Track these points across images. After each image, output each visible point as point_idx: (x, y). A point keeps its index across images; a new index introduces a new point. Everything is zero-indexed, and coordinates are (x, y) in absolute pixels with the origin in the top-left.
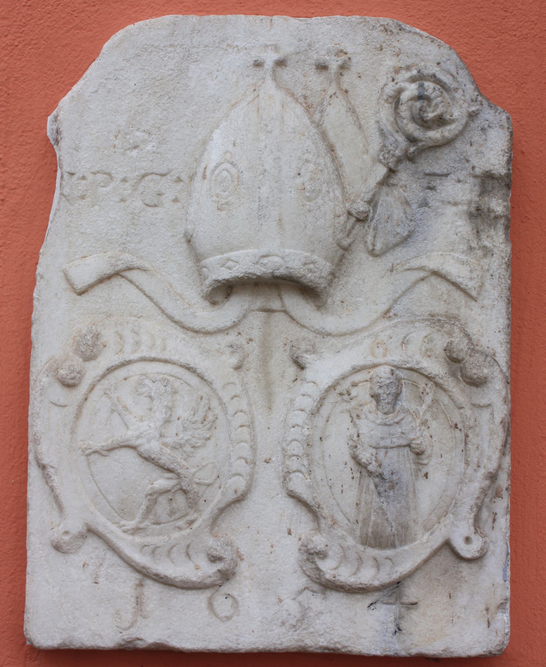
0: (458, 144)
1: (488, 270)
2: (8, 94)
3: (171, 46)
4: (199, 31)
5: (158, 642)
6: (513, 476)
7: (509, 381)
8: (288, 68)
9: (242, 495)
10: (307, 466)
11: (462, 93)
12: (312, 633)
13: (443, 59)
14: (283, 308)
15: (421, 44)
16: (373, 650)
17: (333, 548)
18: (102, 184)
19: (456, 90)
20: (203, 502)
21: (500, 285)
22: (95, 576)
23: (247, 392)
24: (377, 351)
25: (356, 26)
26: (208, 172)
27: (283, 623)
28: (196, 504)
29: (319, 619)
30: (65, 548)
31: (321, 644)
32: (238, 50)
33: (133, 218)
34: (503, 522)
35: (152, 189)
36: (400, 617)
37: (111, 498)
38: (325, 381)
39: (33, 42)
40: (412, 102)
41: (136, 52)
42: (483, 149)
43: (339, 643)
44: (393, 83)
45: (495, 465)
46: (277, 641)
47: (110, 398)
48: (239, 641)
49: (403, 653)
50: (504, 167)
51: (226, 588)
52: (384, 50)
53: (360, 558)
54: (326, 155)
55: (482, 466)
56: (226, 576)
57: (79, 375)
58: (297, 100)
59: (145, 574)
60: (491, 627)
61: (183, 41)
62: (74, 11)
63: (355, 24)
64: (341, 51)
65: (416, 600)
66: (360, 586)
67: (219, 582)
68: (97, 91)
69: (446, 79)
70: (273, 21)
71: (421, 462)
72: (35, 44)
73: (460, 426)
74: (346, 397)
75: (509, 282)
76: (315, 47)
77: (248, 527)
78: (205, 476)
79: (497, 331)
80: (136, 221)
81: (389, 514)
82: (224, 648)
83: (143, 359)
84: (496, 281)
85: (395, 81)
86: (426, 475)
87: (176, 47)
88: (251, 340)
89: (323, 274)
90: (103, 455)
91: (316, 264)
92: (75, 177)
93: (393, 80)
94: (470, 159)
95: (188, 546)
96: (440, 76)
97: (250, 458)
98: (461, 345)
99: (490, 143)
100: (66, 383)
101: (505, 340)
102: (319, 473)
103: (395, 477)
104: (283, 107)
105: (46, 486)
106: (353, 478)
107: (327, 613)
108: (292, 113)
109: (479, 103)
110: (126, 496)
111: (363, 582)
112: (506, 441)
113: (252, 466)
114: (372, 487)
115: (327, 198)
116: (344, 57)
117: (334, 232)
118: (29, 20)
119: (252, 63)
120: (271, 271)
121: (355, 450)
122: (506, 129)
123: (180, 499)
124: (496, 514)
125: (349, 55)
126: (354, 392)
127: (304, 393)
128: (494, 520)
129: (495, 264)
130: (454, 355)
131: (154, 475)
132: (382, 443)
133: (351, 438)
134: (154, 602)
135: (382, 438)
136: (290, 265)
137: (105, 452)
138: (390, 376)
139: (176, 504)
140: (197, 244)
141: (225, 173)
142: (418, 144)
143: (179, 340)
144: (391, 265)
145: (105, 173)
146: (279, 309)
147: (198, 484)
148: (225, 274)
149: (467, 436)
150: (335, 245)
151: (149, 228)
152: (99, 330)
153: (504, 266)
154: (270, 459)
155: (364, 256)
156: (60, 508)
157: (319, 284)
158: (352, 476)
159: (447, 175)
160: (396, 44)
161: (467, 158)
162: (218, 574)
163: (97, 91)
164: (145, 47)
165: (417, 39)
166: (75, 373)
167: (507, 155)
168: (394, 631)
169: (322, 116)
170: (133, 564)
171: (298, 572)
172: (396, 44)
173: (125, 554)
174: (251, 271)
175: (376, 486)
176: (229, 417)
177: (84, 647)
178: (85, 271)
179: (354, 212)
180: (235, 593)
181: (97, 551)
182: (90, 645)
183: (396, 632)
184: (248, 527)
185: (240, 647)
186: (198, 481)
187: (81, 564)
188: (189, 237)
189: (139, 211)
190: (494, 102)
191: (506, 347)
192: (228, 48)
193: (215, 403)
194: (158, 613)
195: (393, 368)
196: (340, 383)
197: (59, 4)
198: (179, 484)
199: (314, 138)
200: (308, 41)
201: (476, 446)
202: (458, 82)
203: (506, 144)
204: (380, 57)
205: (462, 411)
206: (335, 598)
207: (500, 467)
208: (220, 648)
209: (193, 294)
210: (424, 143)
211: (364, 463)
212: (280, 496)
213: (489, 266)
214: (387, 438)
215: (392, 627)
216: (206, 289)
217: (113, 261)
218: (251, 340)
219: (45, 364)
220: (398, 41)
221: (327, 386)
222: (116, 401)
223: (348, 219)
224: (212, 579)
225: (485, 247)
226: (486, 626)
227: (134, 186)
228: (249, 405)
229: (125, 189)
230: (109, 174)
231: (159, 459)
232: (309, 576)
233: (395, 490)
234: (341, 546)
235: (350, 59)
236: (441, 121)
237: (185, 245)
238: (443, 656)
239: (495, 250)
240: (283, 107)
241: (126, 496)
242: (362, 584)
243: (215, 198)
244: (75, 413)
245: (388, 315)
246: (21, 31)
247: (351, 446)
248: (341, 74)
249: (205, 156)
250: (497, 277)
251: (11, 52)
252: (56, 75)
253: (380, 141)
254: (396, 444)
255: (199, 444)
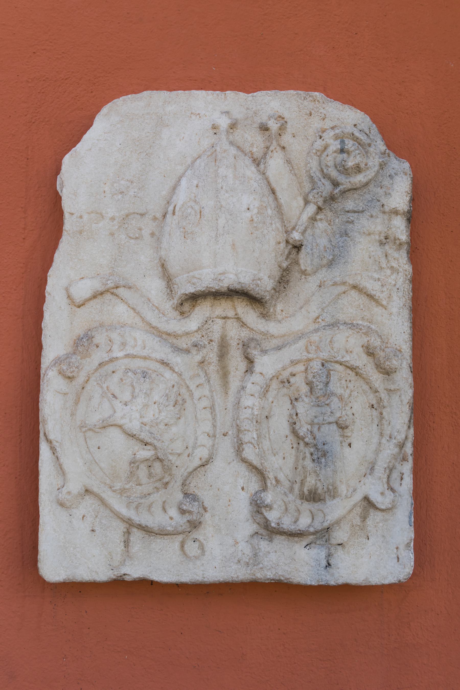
0: (371, 187)
1: (395, 285)
2: (28, 159)
3: (148, 114)
4: (169, 102)
5: (142, 576)
6: (416, 445)
7: (412, 370)
8: (238, 130)
9: (206, 461)
10: (256, 439)
11: (374, 148)
12: (261, 568)
13: (359, 122)
14: (236, 316)
15: (342, 111)
16: (309, 581)
17: (277, 503)
18: (95, 222)
19: (370, 145)
20: (176, 468)
21: (404, 297)
22: (92, 525)
23: (209, 381)
24: (310, 348)
25: (291, 97)
26: (177, 209)
27: (239, 561)
28: (170, 469)
29: (267, 557)
30: (68, 504)
31: (269, 577)
32: (200, 117)
33: (119, 247)
34: (408, 481)
35: (134, 225)
36: (329, 555)
37: (102, 465)
38: (270, 371)
39: (46, 120)
40: (336, 154)
41: (121, 119)
42: (390, 191)
43: (283, 576)
44: (321, 140)
45: (403, 436)
46: (234, 575)
47: (101, 387)
48: (205, 576)
49: (332, 583)
50: (407, 205)
51: (195, 535)
52: (313, 116)
53: (299, 510)
54: (269, 195)
55: (393, 437)
56: (195, 525)
57: (77, 370)
58: (246, 155)
59: (130, 525)
60: (400, 562)
61: (157, 110)
62: (76, 96)
63: (290, 96)
64: (280, 117)
65: (342, 542)
66: (299, 532)
67: (189, 530)
68: (90, 149)
69: (363, 137)
70: (227, 95)
71: (345, 434)
72: (47, 121)
73: (375, 406)
74: (287, 384)
75: (411, 294)
76: (259, 114)
77: (211, 486)
78: (178, 446)
79: (402, 332)
80: (122, 250)
81: (321, 476)
82: (193, 581)
83: (127, 356)
84: (401, 294)
85: (322, 139)
86: (350, 445)
87: (152, 115)
88: (211, 341)
89: (268, 289)
90: (95, 432)
91: (262, 281)
92: (74, 216)
93: (321, 137)
94: (380, 199)
95: (164, 502)
96: (357, 134)
97: (211, 433)
98: (376, 342)
99: (396, 186)
100: (67, 376)
101: (408, 339)
102: (266, 444)
103: (326, 447)
104: (235, 158)
105: (53, 456)
106: (293, 448)
107: (273, 552)
108: (242, 163)
109: (387, 155)
110: (115, 464)
111: (301, 529)
112: (411, 417)
113: (213, 438)
114: (308, 455)
115: (270, 229)
116: (282, 121)
117: (276, 256)
118: (43, 104)
119: (210, 126)
120: (227, 285)
121: (294, 426)
122: (408, 175)
123: (157, 466)
124: (403, 474)
125: (285, 120)
126: (292, 380)
127: (253, 382)
128: (402, 479)
129: (401, 280)
130: (371, 351)
131: (136, 448)
132: (316, 421)
133: (291, 416)
134: (138, 545)
135: (316, 417)
136: (242, 280)
137: (98, 430)
138: (321, 368)
139: (154, 470)
140: (169, 266)
141: (189, 210)
142: (335, 194)
143: (155, 341)
144: (319, 282)
145: (97, 213)
146: (233, 317)
147: (171, 454)
148: (191, 290)
149: (381, 414)
150: (277, 266)
151: (132, 256)
152: (93, 335)
153: (407, 282)
154: (227, 433)
155: (297, 275)
156: (64, 474)
157: (264, 296)
158: (291, 446)
159: (363, 212)
160: (322, 110)
161: (378, 198)
162: (188, 524)
163: (90, 149)
164: (128, 115)
165: (338, 106)
166: (74, 368)
167: (409, 195)
168: (325, 566)
169: (265, 167)
170: (121, 516)
171: (250, 520)
172: (322, 110)
173: (115, 509)
174: (211, 286)
175: (312, 454)
176: (195, 401)
177: (84, 581)
178: (83, 290)
179: (291, 241)
180: (201, 538)
181: (94, 506)
182: (88, 580)
183: (326, 566)
184: (211, 486)
185: (206, 580)
186: (170, 451)
187: (81, 517)
188: (163, 261)
189: (124, 242)
190: (400, 155)
191: (410, 344)
192: (192, 115)
193: (183, 391)
194: (141, 554)
195: (323, 362)
196: (241, 383)
197: (66, 91)
198: (156, 454)
199: (260, 182)
200: (253, 109)
201: (388, 422)
202: (371, 139)
203: (408, 186)
204: (309, 121)
205: (377, 394)
206: (279, 540)
207: (406, 438)
208: (190, 581)
209: (168, 306)
210: (345, 186)
211: (302, 436)
212: (235, 461)
213: (396, 282)
214: (319, 417)
215: (324, 563)
216: (176, 301)
217: (104, 281)
218: (211, 341)
219: (52, 362)
220: (324, 108)
221: (271, 376)
222: (105, 389)
223: (286, 246)
224: (183, 527)
225: (392, 267)
226: (396, 560)
227: (120, 223)
228: (211, 391)
229: (113, 226)
230: (101, 214)
231: (140, 435)
232: (258, 524)
233: (326, 457)
234: (283, 501)
235: (286, 122)
236: (358, 169)
237: (160, 269)
238: (363, 585)
239: (401, 270)
240: (235, 158)
241: (115, 464)
242: (300, 530)
243: (182, 230)
244: (74, 399)
245: (317, 320)
246: (37, 111)
247: (291, 423)
248: (280, 135)
249: (174, 198)
250: (402, 291)
251: (29, 128)
252: (63, 144)
253: (310, 186)
254: (327, 421)
255: (172, 423)
